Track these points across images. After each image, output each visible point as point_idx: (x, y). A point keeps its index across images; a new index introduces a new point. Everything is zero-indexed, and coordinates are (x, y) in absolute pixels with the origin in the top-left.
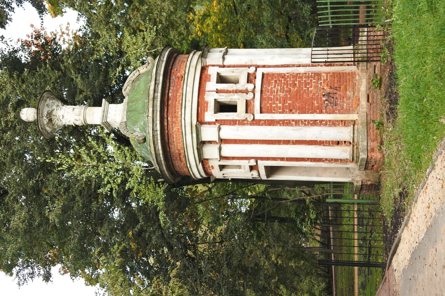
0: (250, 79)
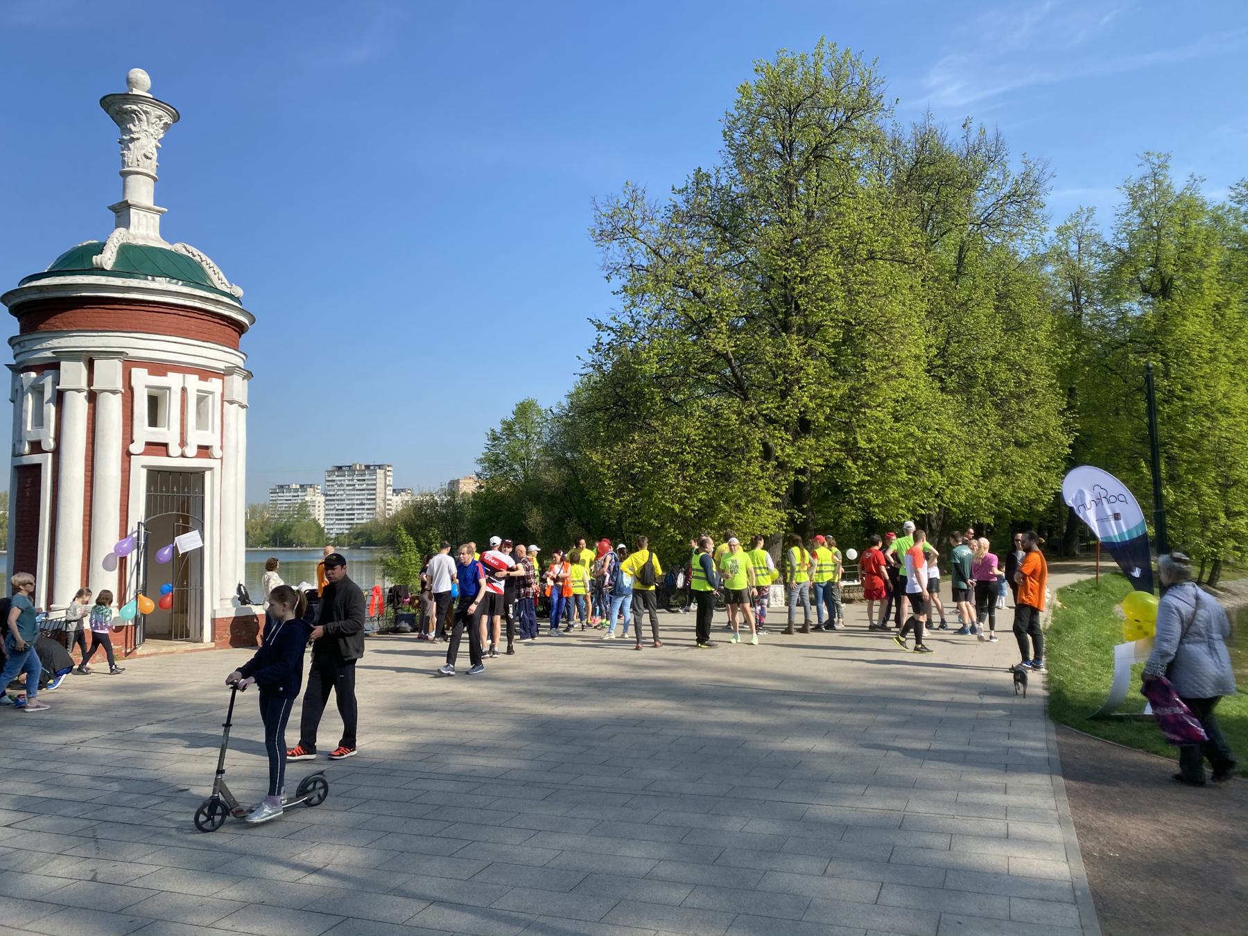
0: (204, 450)
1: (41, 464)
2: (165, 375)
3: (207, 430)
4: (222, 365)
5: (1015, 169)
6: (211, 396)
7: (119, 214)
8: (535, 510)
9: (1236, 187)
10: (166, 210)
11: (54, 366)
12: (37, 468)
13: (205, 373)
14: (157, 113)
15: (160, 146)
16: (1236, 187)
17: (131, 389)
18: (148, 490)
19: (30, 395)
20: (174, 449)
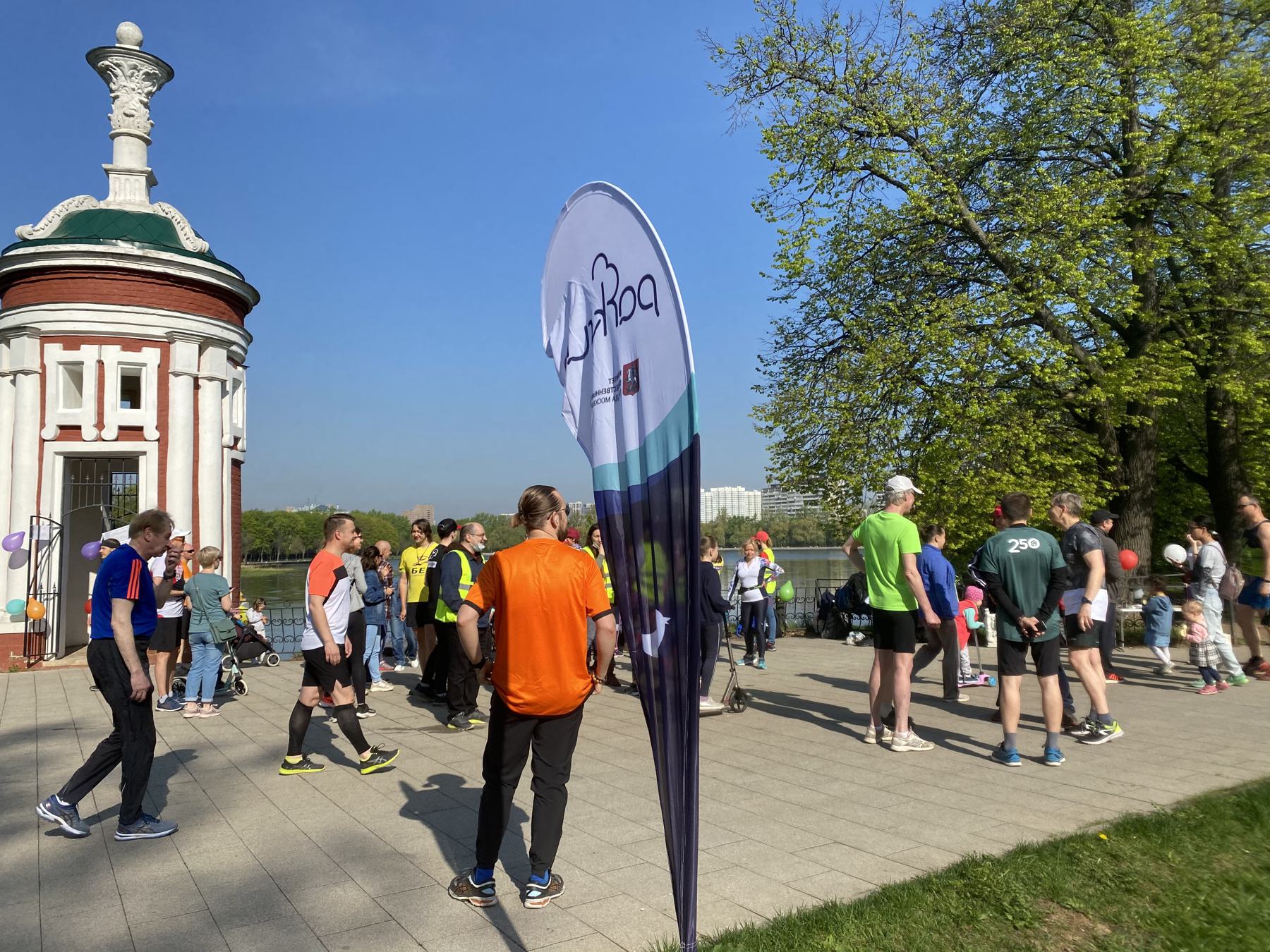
1: (232, 459)
2: (139, 350)
3: (65, 406)
4: (160, 332)
6: (144, 368)
13: (132, 343)
14: (130, 63)
20: (89, 432)
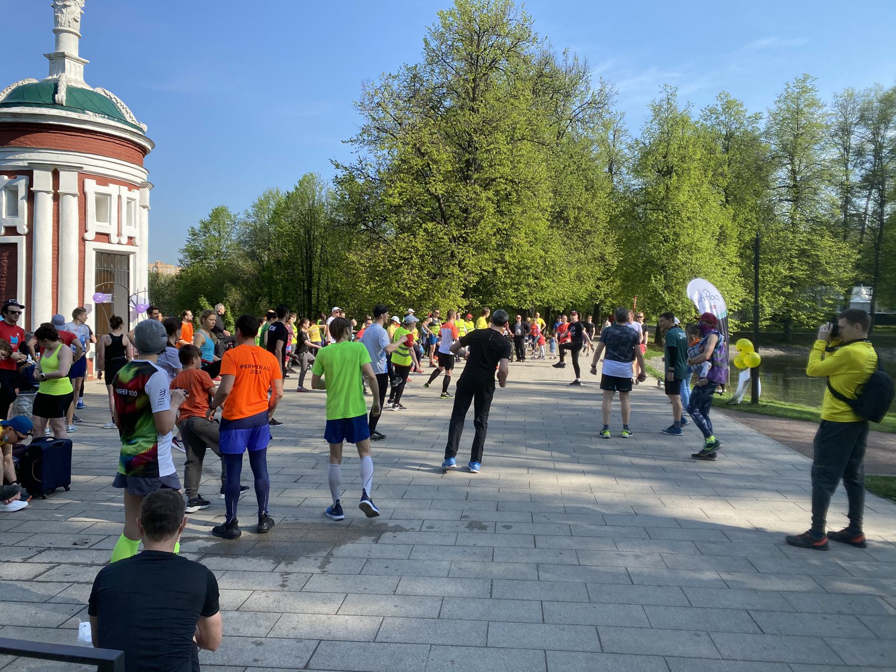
1: (17, 244)
4: (139, 181)
5: (595, 87)
6: (133, 202)
7: (53, 61)
8: (234, 290)
9: (704, 110)
10: (89, 62)
11: (28, 173)
12: (15, 245)
15: (83, 12)
16: (704, 110)
17: (84, 194)
18: (96, 266)
19: (3, 192)
20: (114, 239)
